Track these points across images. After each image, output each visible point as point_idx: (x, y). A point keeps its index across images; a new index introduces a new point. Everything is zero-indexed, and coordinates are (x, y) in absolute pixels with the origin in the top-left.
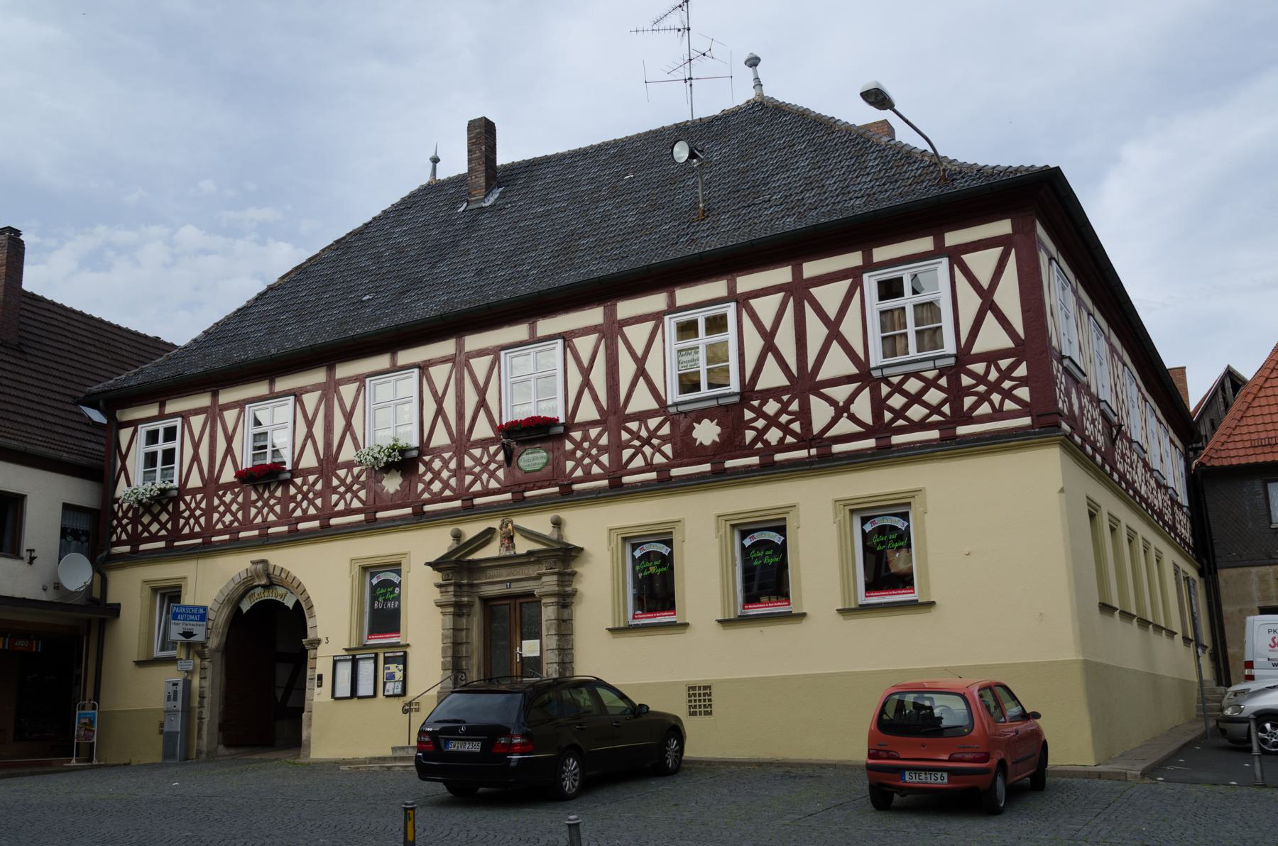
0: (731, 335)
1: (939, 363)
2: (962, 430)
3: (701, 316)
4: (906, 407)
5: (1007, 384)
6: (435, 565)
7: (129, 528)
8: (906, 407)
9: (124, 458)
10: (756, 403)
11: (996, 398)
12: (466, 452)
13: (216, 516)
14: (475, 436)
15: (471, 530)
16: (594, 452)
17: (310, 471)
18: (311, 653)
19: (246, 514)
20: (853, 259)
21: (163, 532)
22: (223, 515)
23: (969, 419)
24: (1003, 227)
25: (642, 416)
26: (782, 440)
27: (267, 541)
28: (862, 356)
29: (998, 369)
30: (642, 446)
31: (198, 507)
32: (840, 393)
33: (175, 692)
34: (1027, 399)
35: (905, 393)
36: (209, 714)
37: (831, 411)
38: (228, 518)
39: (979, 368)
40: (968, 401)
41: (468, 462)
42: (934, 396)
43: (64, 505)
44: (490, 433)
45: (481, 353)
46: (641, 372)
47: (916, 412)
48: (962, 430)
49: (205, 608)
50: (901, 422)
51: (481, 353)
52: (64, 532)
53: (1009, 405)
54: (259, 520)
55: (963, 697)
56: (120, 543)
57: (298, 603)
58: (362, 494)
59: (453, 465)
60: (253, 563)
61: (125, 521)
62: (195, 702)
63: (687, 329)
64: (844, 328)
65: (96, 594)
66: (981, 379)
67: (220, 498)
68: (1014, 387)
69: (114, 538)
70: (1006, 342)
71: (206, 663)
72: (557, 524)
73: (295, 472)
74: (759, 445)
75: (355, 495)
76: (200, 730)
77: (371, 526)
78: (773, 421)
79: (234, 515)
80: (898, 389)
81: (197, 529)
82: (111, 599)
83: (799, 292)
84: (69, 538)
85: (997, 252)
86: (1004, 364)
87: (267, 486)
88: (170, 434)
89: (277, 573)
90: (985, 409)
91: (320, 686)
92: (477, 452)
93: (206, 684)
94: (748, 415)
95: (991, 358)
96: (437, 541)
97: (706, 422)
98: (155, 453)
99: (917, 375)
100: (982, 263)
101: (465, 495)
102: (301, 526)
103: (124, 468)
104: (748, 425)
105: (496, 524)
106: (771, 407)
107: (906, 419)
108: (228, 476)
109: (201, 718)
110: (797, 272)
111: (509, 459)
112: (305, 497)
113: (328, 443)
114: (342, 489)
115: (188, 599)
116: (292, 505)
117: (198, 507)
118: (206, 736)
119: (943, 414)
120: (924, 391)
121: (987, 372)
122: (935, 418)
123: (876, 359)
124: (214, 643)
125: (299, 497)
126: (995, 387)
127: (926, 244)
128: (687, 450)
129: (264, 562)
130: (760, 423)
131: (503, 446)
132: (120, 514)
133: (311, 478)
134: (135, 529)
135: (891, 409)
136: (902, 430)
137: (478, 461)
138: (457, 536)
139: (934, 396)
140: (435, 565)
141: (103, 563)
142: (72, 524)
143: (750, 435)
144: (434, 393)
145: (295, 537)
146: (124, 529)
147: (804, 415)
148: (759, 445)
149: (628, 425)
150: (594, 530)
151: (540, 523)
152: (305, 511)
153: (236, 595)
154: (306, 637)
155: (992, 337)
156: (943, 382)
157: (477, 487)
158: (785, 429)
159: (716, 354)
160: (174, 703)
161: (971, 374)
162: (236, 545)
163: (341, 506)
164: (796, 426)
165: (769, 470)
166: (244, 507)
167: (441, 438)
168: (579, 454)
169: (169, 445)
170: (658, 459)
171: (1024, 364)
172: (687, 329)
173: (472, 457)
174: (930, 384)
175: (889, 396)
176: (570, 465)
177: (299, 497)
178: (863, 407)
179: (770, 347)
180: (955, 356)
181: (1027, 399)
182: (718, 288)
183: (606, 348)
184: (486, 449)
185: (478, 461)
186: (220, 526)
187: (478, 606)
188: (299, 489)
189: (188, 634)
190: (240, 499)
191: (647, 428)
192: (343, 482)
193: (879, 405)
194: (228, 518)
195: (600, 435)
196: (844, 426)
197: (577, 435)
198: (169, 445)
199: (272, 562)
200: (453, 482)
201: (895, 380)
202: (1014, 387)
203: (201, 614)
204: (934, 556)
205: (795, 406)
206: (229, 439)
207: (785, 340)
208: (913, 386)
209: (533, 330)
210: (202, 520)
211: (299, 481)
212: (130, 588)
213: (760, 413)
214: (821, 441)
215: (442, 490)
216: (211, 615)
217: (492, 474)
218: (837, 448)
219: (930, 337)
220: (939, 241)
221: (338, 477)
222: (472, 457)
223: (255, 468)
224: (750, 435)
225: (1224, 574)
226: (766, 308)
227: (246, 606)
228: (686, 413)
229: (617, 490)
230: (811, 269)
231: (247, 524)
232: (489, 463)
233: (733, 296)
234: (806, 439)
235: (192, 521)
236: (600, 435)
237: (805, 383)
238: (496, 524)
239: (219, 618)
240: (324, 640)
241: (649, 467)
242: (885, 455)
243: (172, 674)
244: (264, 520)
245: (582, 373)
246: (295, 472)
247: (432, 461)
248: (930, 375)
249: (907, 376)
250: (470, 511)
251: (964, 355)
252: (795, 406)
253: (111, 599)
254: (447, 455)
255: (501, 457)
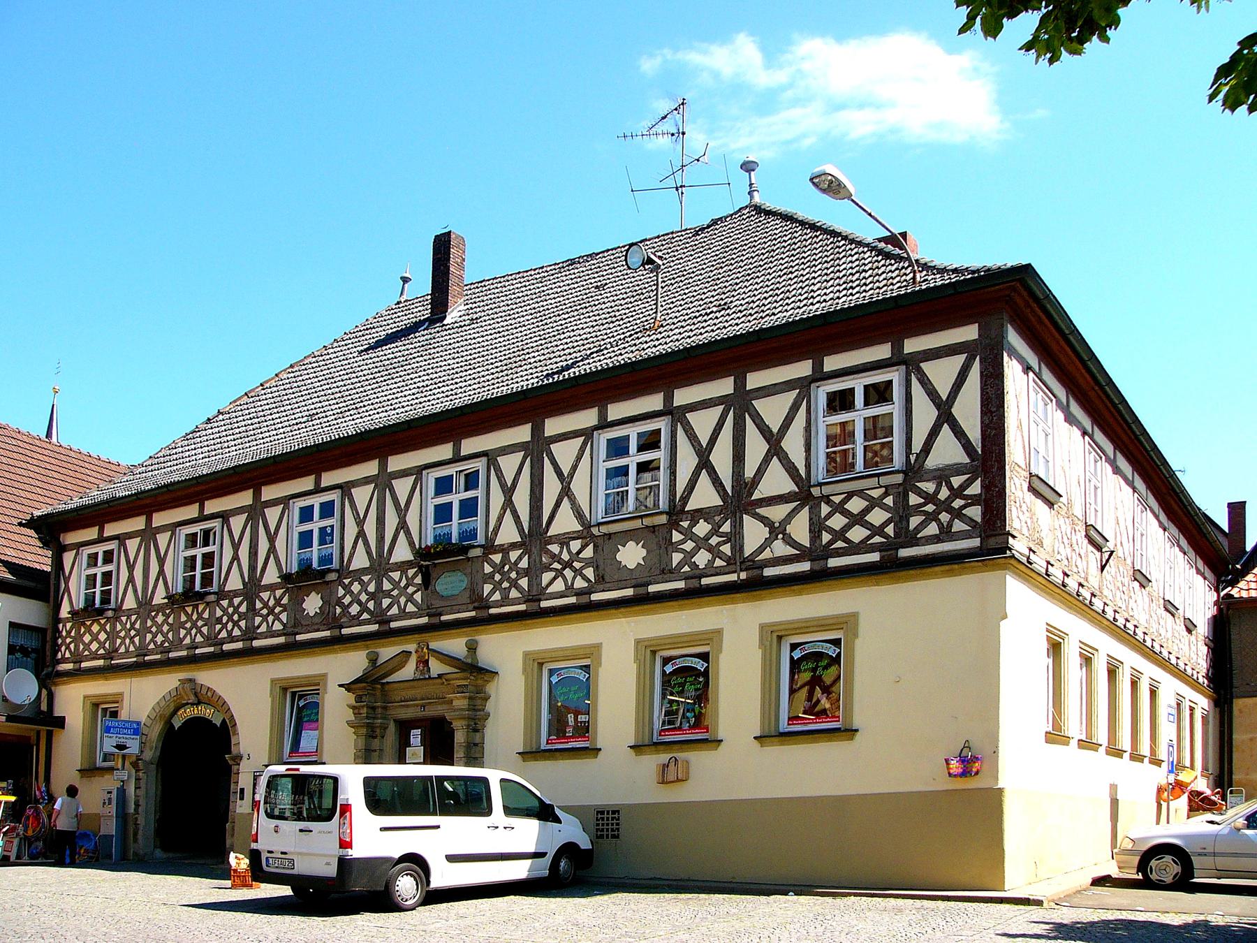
0: (895, 409)
1: (885, 480)
2: (904, 553)
3: (632, 433)
4: (847, 527)
5: (957, 503)
6: (348, 687)
7: (72, 646)
8: (847, 527)
9: (67, 580)
10: (685, 524)
11: (944, 517)
12: (385, 574)
13: (149, 636)
14: (395, 559)
15: (387, 652)
16: (513, 575)
17: (236, 593)
18: (235, 768)
20: (803, 369)
21: (102, 651)
22: (155, 636)
23: (913, 541)
24: (969, 333)
25: (564, 540)
26: (711, 562)
27: (193, 660)
28: (803, 472)
29: (950, 487)
30: (564, 569)
31: (132, 627)
32: (777, 513)
33: (110, 799)
34: (979, 519)
35: (846, 513)
36: (146, 821)
37: (765, 532)
38: (159, 639)
39: (929, 487)
40: (914, 521)
41: (387, 586)
42: (877, 517)
43: (12, 625)
44: (409, 556)
45: (404, 473)
46: (566, 492)
47: (857, 534)
48: (904, 553)
49: (138, 723)
50: (840, 544)
51: (404, 473)
52: (12, 649)
53: (958, 526)
54: (187, 641)
56: (64, 660)
57: (224, 721)
58: (284, 617)
59: (372, 588)
61: (68, 640)
62: (131, 809)
63: (618, 448)
64: (933, 413)
65: (44, 707)
66: (930, 498)
68: (965, 507)
69: (59, 656)
70: (962, 458)
72: (472, 648)
74: (686, 568)
75: (277, 618)
76: (135, 834)
77: (291, 648)
78: (702, 543)
79: (165, 635)
80: (840, 509)
81: (132, 648)
82: (57, 713)
83: (383, 482)
84: (18, 655)
85: (960, 359)
86: (956, 481)
88: (471, 481)
89: (204, 691)
90: (933, 529)
91: (242, 798)
92: (396, 575)
93: (141, 792)
94: (676, 536)
95: (942, 475)
96: (351, 664)
97: (631, 544)
98: (194, 558)
99: (860, 493)
100: (942, 373)
101: (381, 617)
102: (226, 647)
103: (67, 589)
104: (675, 547)
105: (412, 647)
106: (702, 528)
107: (847, 540)
108: (159, 598)
109: (136, 824)
110: (740, 383)
111: (426, 583)
112: (230, 619)
113: (252, 567)
114: (265, 612)
115: (124, 715)
116: (218, 627)
117: (132, 627)
118: (144, 840)
119: (886, 536)
120: (867, 511)
121: (937, 491)
122: (877, 539)
123: (819, 473)
124: (148, 755)
125: (225, 619)
126: (946, 506)
127: (882, 351)
128: (607, 573)
129: (191, 681)
130: (689, 546)
131: (420, 567)
132: (64, 633)
133: (237, 601)
134: (77, 647)
135: (830, 530)
136: (839, 553)
137: (396, 585)
138: (373, 660)
139: (877, 517)
140: (348, 687)
141: (48, 676)
142: (20, 641)
143: (677, 558)
144: (503, 484)
145: (220, 657)
146: (68, 647)
147: (736, 537)
148: (686, 568)
150: (505, 650)
151: (455, 645)
152: (230, 633)
153: (168, 713)
154: (230, 752)
155: (947, 452)
156: (889, 501)
157: (394, 610)
158: (715, 552)
159: (876, 428)
161: (920, 493)
163: (263, 628)
164: (726, 549)
165: (696, 593)
166: (175, 628)
168: (497, 577)
169: (306, 527)
170: (580, 584)
172: (841, 401)
173: (391, 580)
174: (874, 503)
175: (829, 516)
176: (488, 588)
177: (225, 619)
178: (800, 529)
179: (704, 464)
181: (979, 519)
182: (654, 402)
183: (984, 376)
184: (404, 572)
185: (396, 585)
186: (152, 646)
187: (392, 727)
188: (225, 611)
189: (121, 747)
190: (171, 620)
191: (569, 552)
192: (266, 605)
193: (817, 527)
194: (159, 639)
195: (520, 558)
196: (780, 548)
197: (497, 558)
198: (306, 527)
200: (371, 605)
201: (837, 499)
202: (965, 507)
203: (136, 729)
204: (868, 686)
205: (726, 528)
206: (272, 539)
207: (722, 458)
208: (856, 505)
209: (457, 449)
210: (137, 640)
211: (225, 603)
212: (72, 700)
213: (688, 534)
214: (751, 564)
215: (360, 613)
217: (410, 599)
218: (769, 572)
219: (877, 457)
220: (897, 348)
221: (262, 600)
222: (391, 580)
224: (677, 558)
225: (1239, 704)
226: (703, 423)
227: (177, 723)
228: (609, 536)
229: (535, 614)
230: (755, 380)
231: (178, 643)
232: (406, 587)
233: (669, 411)
234: (738, 560)
235: (127, 641)
236: (520, 558)
237: (741, 499)
238: (412, 647)
239: (155, 732)
240: (246, 757)
241: (570, 590)
242: (820, 577)
243: (110, 783)
244: (193, 641)
245: (938, 406)
247: (351, 583)
248: (876, 493)
249: (850, 495)
250: (387, 634)
251: (913, 471)
252: (726, 528)
253: (57, 713)
254: (366, 578)
255: (418, 580)
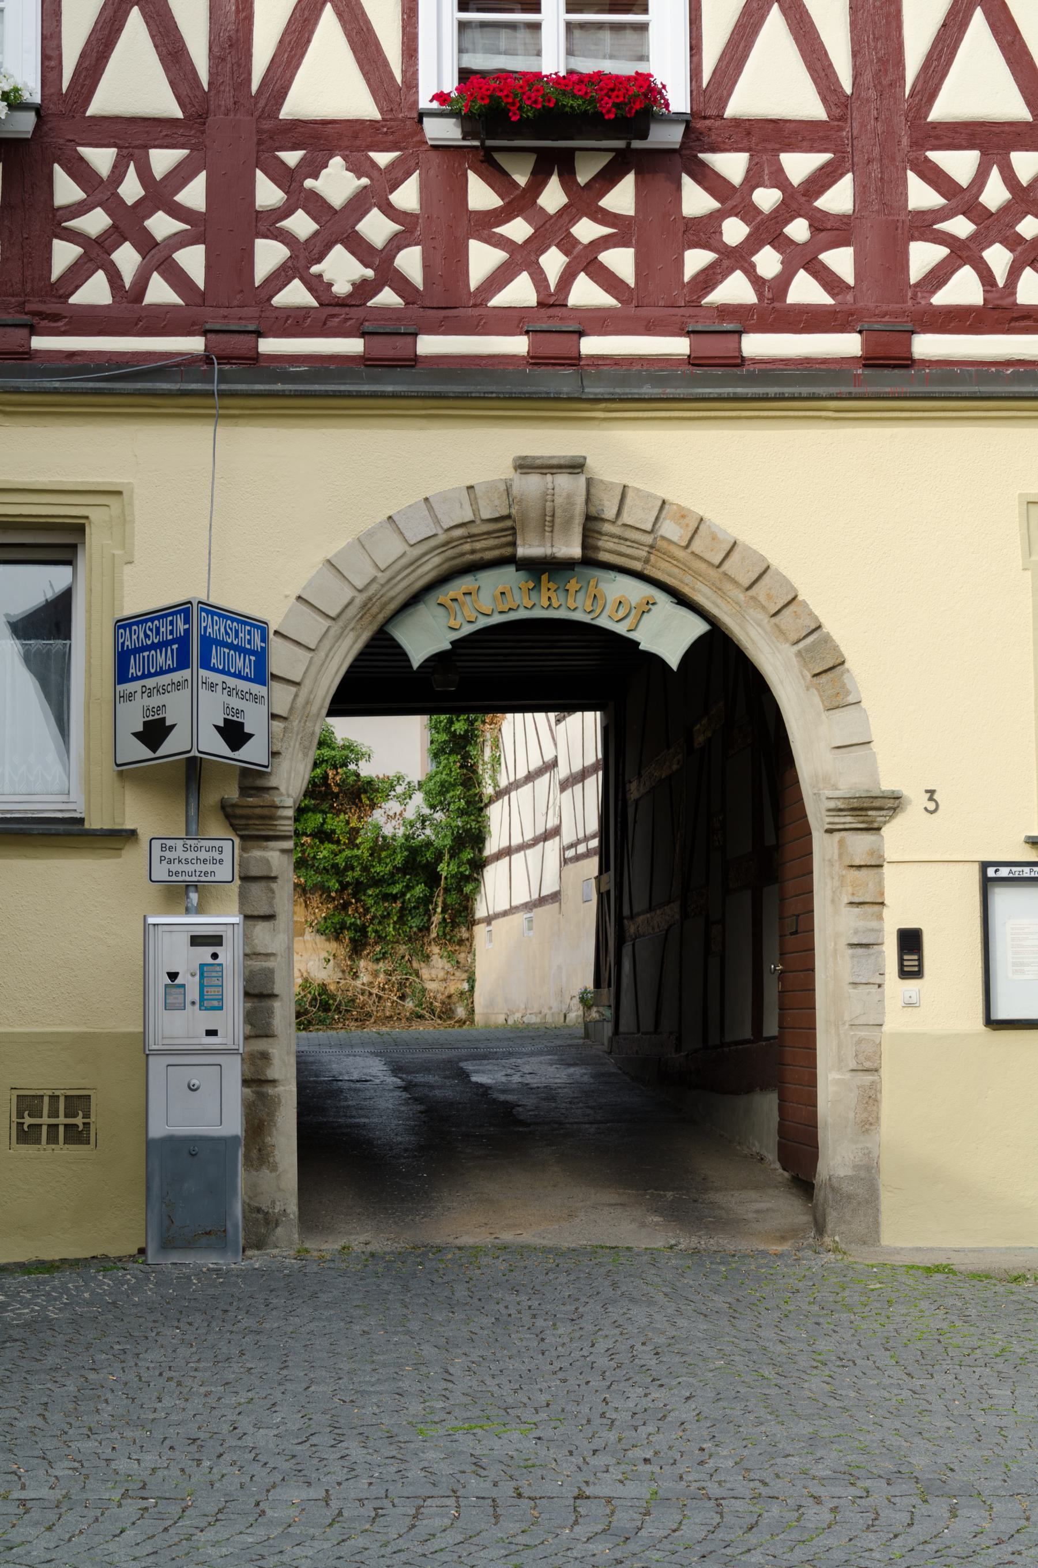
19: (449, 263)
27: (554, 377)
55: (799, 1417)
60: (525, 466)
67: (288, 179)
71: (276, 858)
73: (707, 127)
87: (554, 163)
145: (719, 380)
149: (939, 157)
160: (211, 1019)
161: (936, 178)
162: (388, 375)
167: (135, 83)
171: (847, 180)
180: (38, 109)
181: (688, 183)
199: (599, 467)
216: (282, 659)
223: (573, 80)
231: (450, 302)
240: (917, 801)
246: (707, 127)
